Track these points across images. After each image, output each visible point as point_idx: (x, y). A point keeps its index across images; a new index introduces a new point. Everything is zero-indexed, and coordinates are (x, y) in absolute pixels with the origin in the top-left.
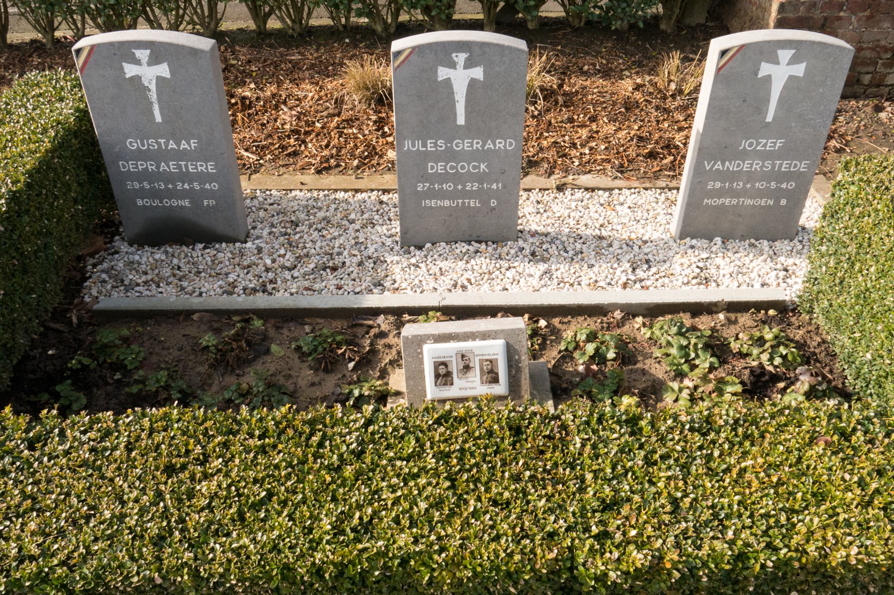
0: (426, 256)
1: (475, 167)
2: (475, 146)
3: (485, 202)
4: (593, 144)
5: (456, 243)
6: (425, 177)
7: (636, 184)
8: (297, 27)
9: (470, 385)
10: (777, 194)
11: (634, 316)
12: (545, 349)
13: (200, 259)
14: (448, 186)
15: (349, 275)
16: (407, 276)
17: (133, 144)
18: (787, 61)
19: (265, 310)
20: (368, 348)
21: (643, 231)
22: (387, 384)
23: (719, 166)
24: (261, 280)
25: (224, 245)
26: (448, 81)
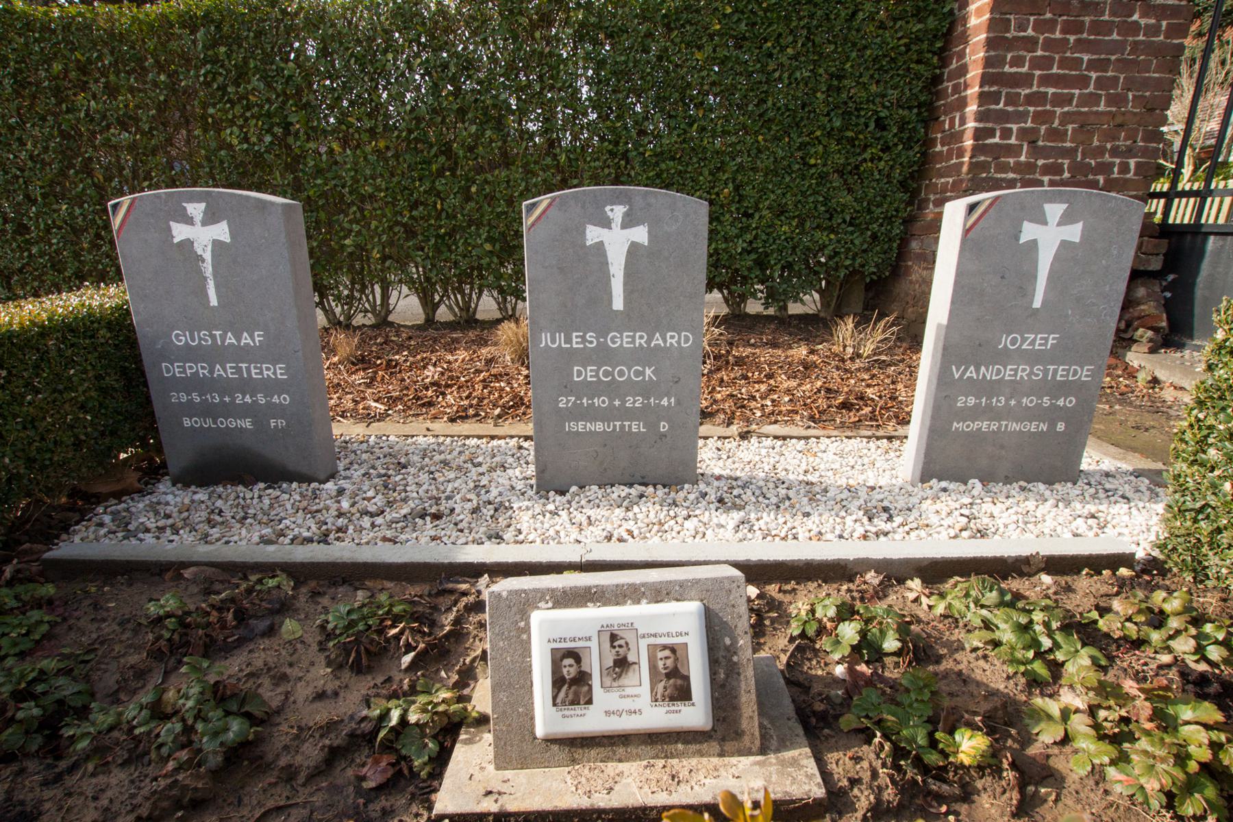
0: (569, 502)
1: (637, 373)
2: (638, 341)
3: (652, 426)
4: (775, 397)
5: (612, 485)
6: (569, 388)
7: (835, 433)
8: (464, 314)
9: (627, 704)
10: (1051, 415)
11: (901, 581)
12: (764, 635)
13: (256, 500)
14: (601, 402)
15: (456, 524)
16: (538, 525)
17: (180, 339)
18: (1057, 219)
19: (303, 564)
20: (448, 628)
21: (863, 477)
22: (468, 699)
23: (971, 373)
24: (324, 527)
25: (295, 485)
26: (600, 245)
